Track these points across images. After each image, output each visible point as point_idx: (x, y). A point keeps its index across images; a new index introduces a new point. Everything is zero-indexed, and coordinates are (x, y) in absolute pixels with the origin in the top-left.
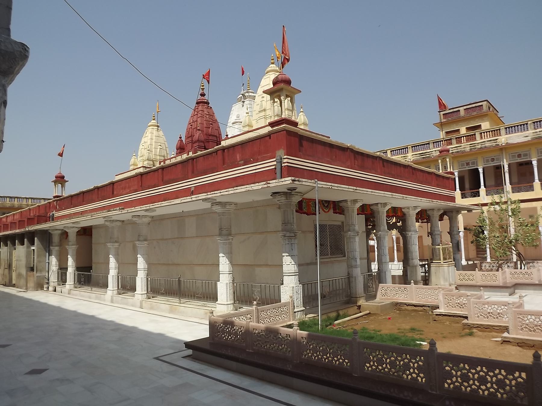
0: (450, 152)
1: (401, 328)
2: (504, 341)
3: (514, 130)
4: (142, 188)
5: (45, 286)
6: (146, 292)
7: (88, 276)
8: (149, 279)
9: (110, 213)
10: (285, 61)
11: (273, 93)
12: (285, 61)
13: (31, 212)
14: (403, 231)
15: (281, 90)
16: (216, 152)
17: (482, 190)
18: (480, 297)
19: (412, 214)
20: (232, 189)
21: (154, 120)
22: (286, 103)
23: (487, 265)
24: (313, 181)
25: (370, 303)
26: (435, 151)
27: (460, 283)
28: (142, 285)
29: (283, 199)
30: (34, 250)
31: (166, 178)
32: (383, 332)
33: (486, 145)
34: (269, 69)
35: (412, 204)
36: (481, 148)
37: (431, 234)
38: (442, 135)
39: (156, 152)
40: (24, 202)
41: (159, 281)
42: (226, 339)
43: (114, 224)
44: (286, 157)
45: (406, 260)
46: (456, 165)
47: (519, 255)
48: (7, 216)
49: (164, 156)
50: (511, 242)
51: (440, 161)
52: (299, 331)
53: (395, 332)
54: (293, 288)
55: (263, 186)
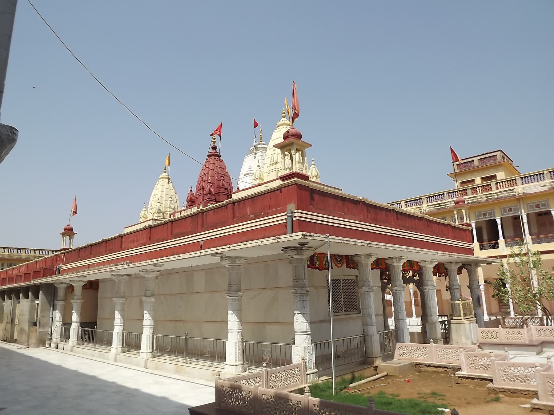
0: (466, 202)
1: (422, 392)
2: (534, 408)
3: (530, 180)
4: (151, 241)
5: (48, 342)
6: (151, 351)
7: (92, 332)
8: (155, 336)
9: (117, 267)
10: (295, 116)
11: (283, 147)
12: (295, 116)
13: (38, 264)
14: (420, 284)
15: (291, 144)
16: (227, 205)
17: (501, 241)
18: (504, 359)
19: (429, 268)
20: (242, 244)
21: (165, 172)
22: (297, 157)
23: (511, 321)
24: (324, 236)
25: (387, 364)
26: (451, 201)
27: (483, 341)
28: (147, 343)
29: (294, 254)
30: (38, 304)
31: (176, 231)
32: (401, 397)
33: (503, 195)
34: (280, 123)
35: (428, 257)
36: (498, 198)
37: (449, 288)
38: (457, 186)
39: (166, 204)
40: (32, 254)
41: (165, 338)
42: (234, 405)
43: (121, 278)
44: (297, 211)
45: (424, 315)
46: (472, 216)
47: (544, 310)
48: (13, 269)
49: (174, 209)
50: (534, 296)
51: (455, 212)
52: (310, 398)
53: (416, 396)
54: (305, 348)
55: (273, 241)
